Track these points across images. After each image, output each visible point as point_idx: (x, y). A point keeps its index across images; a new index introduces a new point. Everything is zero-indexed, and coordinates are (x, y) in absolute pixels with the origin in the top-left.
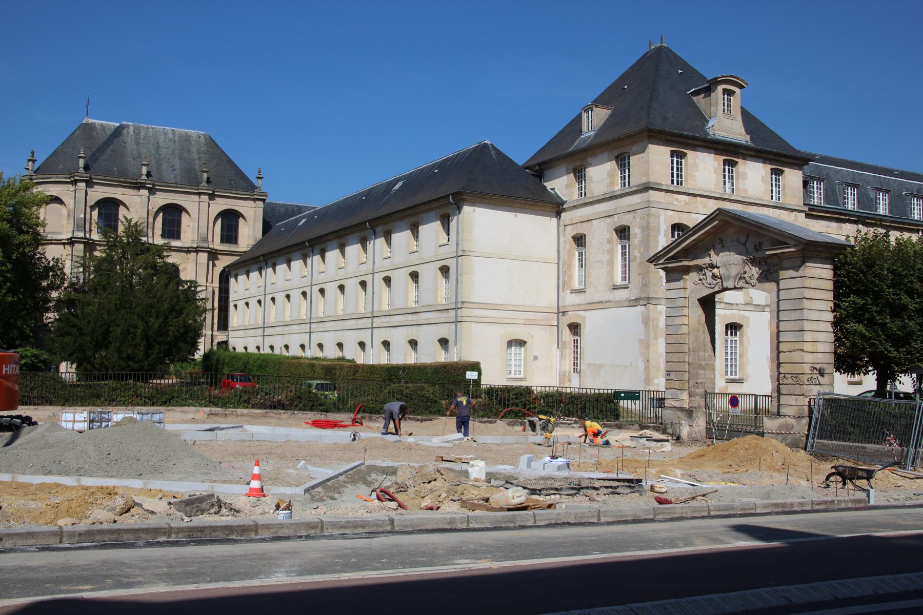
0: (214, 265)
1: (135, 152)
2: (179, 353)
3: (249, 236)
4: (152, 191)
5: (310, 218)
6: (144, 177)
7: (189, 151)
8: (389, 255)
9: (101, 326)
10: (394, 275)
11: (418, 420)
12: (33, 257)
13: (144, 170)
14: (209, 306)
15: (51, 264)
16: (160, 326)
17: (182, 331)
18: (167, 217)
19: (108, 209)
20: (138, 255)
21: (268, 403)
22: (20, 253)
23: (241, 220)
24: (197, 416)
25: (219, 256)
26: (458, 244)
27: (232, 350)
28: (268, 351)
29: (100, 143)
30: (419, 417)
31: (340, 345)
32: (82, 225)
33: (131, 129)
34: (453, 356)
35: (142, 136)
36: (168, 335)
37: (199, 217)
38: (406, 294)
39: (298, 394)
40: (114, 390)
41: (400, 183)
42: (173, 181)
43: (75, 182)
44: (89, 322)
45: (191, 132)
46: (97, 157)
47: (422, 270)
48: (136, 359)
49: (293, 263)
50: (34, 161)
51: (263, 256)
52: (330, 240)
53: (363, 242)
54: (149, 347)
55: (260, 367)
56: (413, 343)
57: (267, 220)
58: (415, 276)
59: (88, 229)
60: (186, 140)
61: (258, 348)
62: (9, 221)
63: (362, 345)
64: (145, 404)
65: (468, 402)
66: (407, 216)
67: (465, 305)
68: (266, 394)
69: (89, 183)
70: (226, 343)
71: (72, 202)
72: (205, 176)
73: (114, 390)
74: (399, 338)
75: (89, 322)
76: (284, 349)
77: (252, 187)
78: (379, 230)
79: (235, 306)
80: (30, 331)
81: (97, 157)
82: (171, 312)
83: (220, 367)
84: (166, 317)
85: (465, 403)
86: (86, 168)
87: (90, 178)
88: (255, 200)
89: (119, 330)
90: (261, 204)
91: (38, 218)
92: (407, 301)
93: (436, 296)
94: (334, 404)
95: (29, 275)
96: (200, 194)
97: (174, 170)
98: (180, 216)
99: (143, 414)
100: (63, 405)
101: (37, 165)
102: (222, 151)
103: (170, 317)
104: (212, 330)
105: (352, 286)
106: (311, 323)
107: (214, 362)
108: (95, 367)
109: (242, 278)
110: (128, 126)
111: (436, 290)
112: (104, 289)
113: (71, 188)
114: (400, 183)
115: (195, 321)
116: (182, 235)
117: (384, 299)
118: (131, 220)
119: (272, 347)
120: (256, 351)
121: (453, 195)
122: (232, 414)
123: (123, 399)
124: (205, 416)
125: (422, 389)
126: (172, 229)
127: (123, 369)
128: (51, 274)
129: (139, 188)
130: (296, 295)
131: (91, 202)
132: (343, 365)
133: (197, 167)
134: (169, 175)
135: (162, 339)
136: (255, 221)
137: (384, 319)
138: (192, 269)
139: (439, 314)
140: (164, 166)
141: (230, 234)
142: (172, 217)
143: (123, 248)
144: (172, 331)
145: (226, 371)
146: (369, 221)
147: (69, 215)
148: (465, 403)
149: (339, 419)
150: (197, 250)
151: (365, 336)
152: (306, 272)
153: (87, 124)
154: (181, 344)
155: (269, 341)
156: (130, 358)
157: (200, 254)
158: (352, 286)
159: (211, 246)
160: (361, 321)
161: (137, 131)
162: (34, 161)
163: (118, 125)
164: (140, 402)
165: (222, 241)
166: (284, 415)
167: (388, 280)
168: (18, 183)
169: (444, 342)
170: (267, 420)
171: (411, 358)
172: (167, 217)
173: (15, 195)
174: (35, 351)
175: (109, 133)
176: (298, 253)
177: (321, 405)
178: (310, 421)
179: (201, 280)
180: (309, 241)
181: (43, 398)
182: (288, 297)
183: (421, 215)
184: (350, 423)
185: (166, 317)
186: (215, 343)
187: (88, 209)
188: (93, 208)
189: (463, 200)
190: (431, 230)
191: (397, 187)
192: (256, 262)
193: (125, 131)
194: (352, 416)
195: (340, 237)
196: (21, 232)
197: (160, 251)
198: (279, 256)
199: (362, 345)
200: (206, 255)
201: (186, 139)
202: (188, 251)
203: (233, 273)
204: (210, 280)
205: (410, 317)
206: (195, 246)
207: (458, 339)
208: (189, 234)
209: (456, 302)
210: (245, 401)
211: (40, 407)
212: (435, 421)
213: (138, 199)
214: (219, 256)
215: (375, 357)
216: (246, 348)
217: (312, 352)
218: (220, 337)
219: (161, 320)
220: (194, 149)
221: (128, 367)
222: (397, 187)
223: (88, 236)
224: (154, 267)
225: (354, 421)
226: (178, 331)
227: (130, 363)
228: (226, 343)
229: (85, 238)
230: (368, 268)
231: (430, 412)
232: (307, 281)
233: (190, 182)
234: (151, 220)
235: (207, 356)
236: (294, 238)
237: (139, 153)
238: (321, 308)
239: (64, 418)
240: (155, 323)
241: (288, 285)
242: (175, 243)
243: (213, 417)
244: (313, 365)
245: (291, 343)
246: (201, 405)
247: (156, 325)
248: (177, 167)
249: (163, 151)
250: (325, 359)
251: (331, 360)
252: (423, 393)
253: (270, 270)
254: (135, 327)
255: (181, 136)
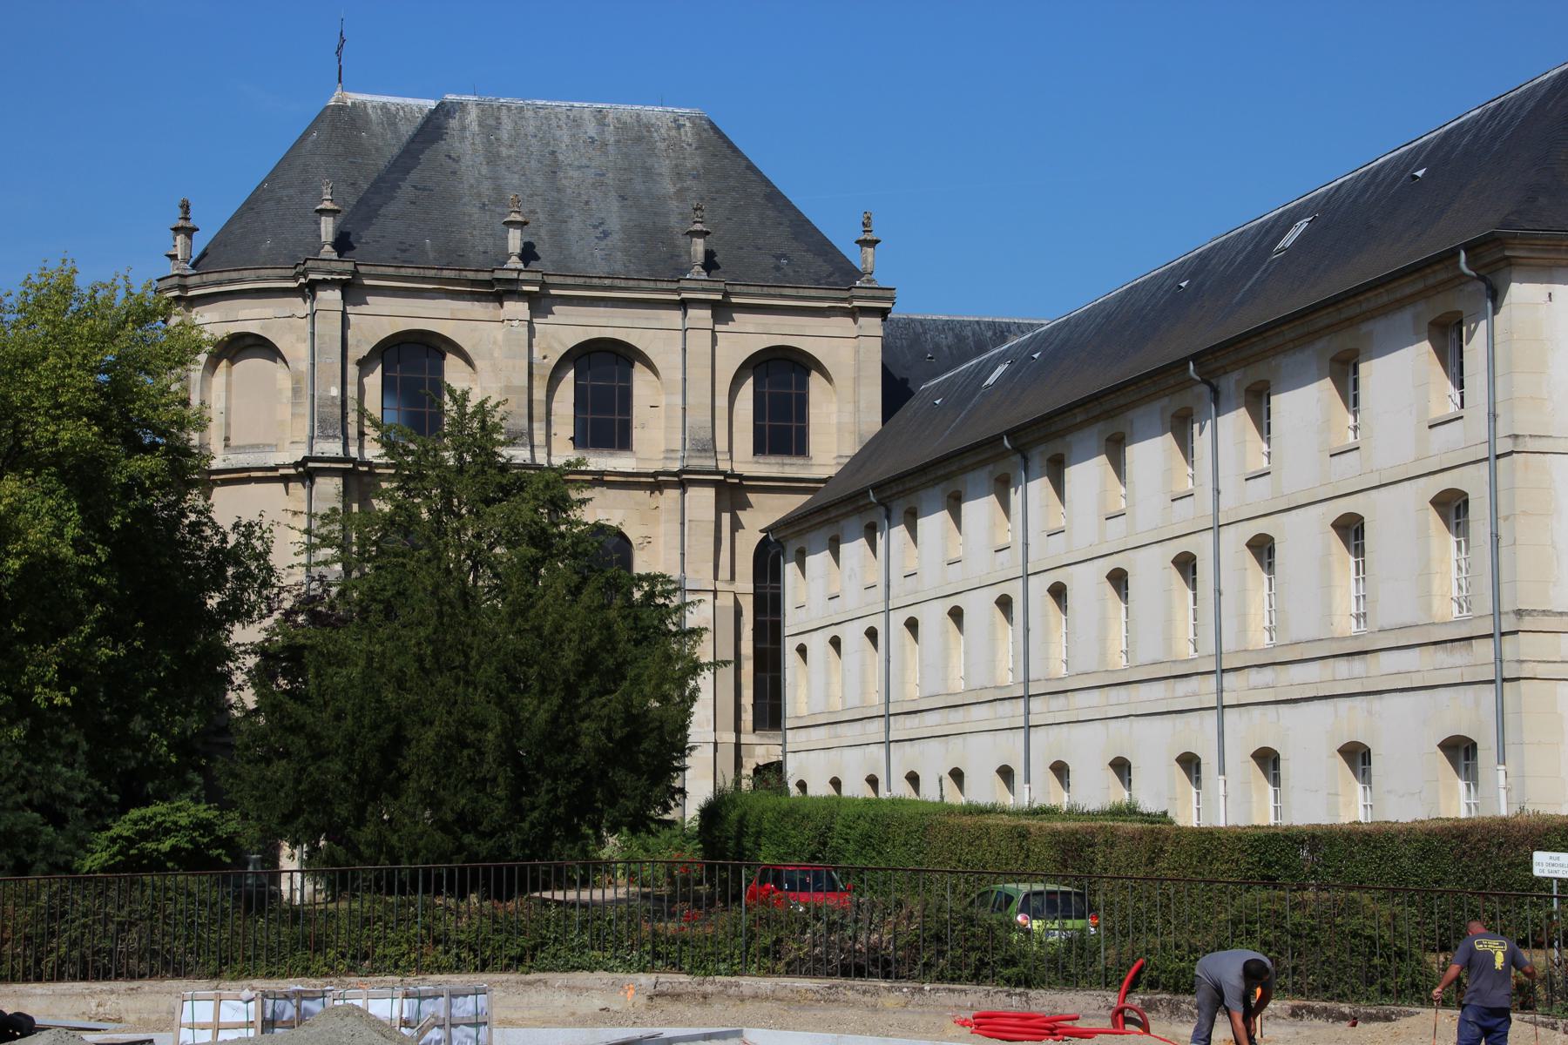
0: (736, 525)
1: (486, 187)
2: (612, 805)
3: (840, 427)
4: (540, 304)
5: (1020, 361)
6: (515, 263)
7: (648, 173)
8: (1264, 464)
9: (375, 727)
10: (1281, 529)
11: (1342, 1017)
12: (173, 524)
13: (515, 240)
14: (704, 653)
15: (232, 540)
16: (554, 720)
17: (618, 734)
18: (587, 382)
19: (413, 361)
20: (488, 502)
21: (837, 957)
22: (133, 513)
23: (815, 381)
24: (617, 1002)
25: (752, 497)
26: (1493, 416)
27: (794, 791)
28: (902, 790)
29: (382, 164)
30: (1346, 1008)
31: (1121, 767)
32: (339, 418)
33: (473, 115)
34: (1496, 798)
35: (505, 136)
36: (576, 745)
37: (687, 379)
38: (1325, 593)
39: (933, 925)
40: (367, 921)
41: (1302, 225)
42: (602, 268)
43: (309, 290)
44: (339, 716)
45: (653, 112)
46: (370, 210)
47: (1375, 509)
48: (485, 826)
49: (968, 508)
50: (189, 232)
51: (877, 487)
52: (1079, 427)
53: (1181, 427)
54: (522, 783)
55: (866, 841)
56: (1357, 756)
57: (898, 373)
58: (1351, 530)
59: (353, 431)
60: (639, 140)
61: (873, 781)
62: (97, 417)
63: (1190, 764)
64: (458, 967)
65: (1512, 960)
66: (1314, 335)
67: (1528, 623)
68: (831, 927)
69: (353, 291)
70: (777, 768)
71: (304, 350)
72: (699, 246)
73: (367, 921)
74: (1308, 739)
75: (339, 716)
76: (949, 783)
77: (846, 274)
78: (1230, 383)
79: (802, 650)
80: (170, 748)
81: (370, 210)
82: (584, 675)
83: (748, 843)
84: (571, 691)
85: (1499, 960)
86: (343, 244)
87: (355, 273)
88: (854, 313)
89: (430, 735)
90: (873, 325)
91: (185, 403)
92: (1328, 615)
93: (1427, 595)
94: (1054, 960)
95: (163, 574)
96: (684, 305)
97: (606, 234)
98: (628, 378)
99: (421, 997)
100: (216, 975)
101: (201, 242)
102: (751, 167)
103: (584, 692)
104: (738, 730)
105: (1152, 573)
106: (1028, 697)
107: (732, 832)
108: (359, 856)
109: (818, 561)
110: (462, 106)
111: (1425, 574)
112: (389, 612)
113: (299, 306)
114: (1302, 225)
115: (665, 699)
116: (637, 434)
117: (1254, 610)
118: (465, 394)
119: (913, 779)
120: (867, 792)
121: (1468, 247)
122: (723, 993)
123: (390, 951)
124: (644, 1000)
125: (1351, 908)
126: (605, 422)
127: (444, 857)
128: (230, 571)
129: (499, 298)
130: (980, 608)
131: (359, 350)
132: (1113, 831)
133: (673, 220)
134: (591, 254)
135: (561, 759)
136: (857, 380)
137: (1256, 677)
138: (671, 543)
139: (1440, 656)
140: (575, 225)
141: (782, 428)
142: (603, 375)
143: (443, 482)
144: (589, 735)
145: (767, 856)
146: (1195, 357)
147: (296, 391)
148: (1499, 960)
149: (1070, 1011)
150: (682, 481)
151: (1198, 735)
152: (1009, 533)
153: (341, 109)
154: (619, 775)
155: (905, 758)
156: (467, 821)
157: (693, 492)
158: (1152, 573)
159: (724, 466)
160: (1182, 687)
161: (490, 122)
162: (189, 232)
163: (432, 104)
164: (443, 960)
165: (759, 449)
166: (890, 995)
167: (1263, 548)
168: (120, 300)
169: (1460, 751)
170: (834, 1012)
171: (1351, 806)
172: (587, 382)
173: (111, 337)
174: (204, 812)
175: (407, 130)
176: (983, 476)
177: (1010, 962)
178: (969, 1015)
179: (698, 574)
180: (1011, 433)
181: (154, 954)
182: (956, 614)
183: (1365, 328)
184: (1107, 1024)
185: (571, 691)
186: (748, 770)
187: (353, 371)
188: (365, 365)
189: (1509, 262)
190: (1401, 374)
191: (1288, 240)
192: (858, 510)
193: (453, 123)
194: (1113, 998)
195: (1109, 415)
196: (135, 447)
197: (556, 489)
198: (925, 486)
199: (1190, 764)
200: (709, 494)
201: (638, 135)
202: (655, 483)
203: (791, 548)
204: (724, 573)
205: (1342, 667)
206: (676, 466)
207: (1510, 737)
208: (655, 438)
209: (1497, 613)
210: (766, 951)
211: (146, 985)
212: (1403, 1023)
213: (497, 332)
214: (752, 497)
215: (1233, 803)
216: (836, 783)
217: (1040, 791)
218: (761, 750)
219: (556, 700)
220: (664, 166)
221: (460, 848)
222: (1288, 240)
223: (354, 452)
224: (541, 539)
225: (1121, 1019)
226: (608, 732)
227: (468, 839)
228: (777, 768)
229: (346, 459)
230: (1198, 511)
231: (1385, 991)
232: (1010, 564)
233: (656, 275)
234: (540, 394)
235: (711, 813)
236: (984, 424)
237: (498, 189)
238: (1058, 648)
239: (186, 1018)
240: (538, 711)
241: (956, 578)
242: (598, 461)
243: (658, 1000)
244: (1023, 834)
245: (970, 765)
246: (628, 966)
247: (543, 716)
248: (614, 224)
249: (570, 178)
250: (1072, 813)
251: (1092, 815)
252: (1355, 922)
253: (899, 533)
254: (481, 726)
255: (622, 127)
